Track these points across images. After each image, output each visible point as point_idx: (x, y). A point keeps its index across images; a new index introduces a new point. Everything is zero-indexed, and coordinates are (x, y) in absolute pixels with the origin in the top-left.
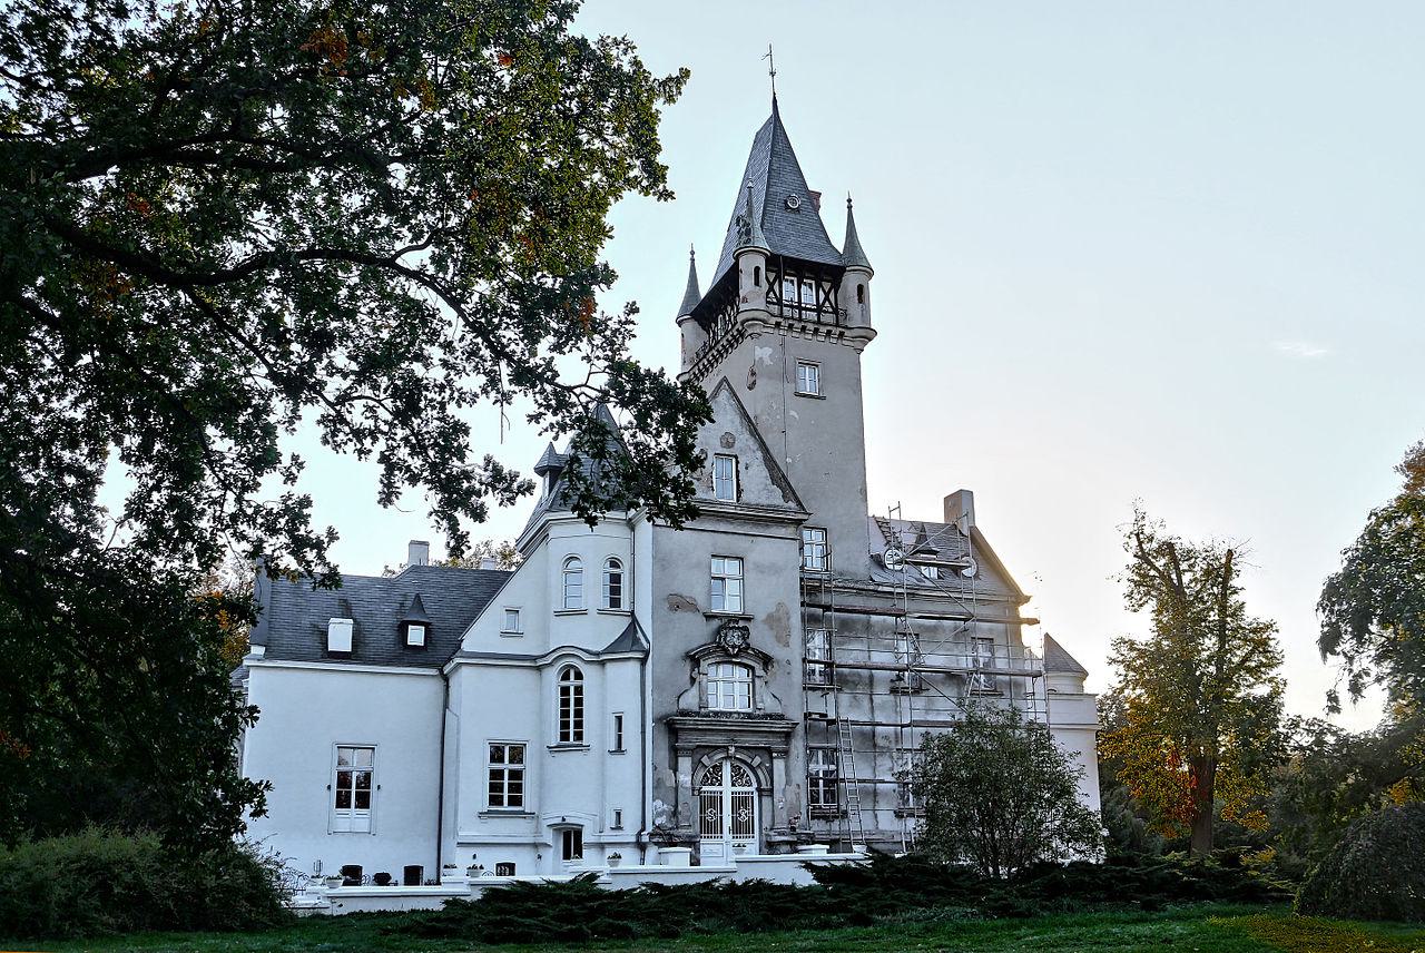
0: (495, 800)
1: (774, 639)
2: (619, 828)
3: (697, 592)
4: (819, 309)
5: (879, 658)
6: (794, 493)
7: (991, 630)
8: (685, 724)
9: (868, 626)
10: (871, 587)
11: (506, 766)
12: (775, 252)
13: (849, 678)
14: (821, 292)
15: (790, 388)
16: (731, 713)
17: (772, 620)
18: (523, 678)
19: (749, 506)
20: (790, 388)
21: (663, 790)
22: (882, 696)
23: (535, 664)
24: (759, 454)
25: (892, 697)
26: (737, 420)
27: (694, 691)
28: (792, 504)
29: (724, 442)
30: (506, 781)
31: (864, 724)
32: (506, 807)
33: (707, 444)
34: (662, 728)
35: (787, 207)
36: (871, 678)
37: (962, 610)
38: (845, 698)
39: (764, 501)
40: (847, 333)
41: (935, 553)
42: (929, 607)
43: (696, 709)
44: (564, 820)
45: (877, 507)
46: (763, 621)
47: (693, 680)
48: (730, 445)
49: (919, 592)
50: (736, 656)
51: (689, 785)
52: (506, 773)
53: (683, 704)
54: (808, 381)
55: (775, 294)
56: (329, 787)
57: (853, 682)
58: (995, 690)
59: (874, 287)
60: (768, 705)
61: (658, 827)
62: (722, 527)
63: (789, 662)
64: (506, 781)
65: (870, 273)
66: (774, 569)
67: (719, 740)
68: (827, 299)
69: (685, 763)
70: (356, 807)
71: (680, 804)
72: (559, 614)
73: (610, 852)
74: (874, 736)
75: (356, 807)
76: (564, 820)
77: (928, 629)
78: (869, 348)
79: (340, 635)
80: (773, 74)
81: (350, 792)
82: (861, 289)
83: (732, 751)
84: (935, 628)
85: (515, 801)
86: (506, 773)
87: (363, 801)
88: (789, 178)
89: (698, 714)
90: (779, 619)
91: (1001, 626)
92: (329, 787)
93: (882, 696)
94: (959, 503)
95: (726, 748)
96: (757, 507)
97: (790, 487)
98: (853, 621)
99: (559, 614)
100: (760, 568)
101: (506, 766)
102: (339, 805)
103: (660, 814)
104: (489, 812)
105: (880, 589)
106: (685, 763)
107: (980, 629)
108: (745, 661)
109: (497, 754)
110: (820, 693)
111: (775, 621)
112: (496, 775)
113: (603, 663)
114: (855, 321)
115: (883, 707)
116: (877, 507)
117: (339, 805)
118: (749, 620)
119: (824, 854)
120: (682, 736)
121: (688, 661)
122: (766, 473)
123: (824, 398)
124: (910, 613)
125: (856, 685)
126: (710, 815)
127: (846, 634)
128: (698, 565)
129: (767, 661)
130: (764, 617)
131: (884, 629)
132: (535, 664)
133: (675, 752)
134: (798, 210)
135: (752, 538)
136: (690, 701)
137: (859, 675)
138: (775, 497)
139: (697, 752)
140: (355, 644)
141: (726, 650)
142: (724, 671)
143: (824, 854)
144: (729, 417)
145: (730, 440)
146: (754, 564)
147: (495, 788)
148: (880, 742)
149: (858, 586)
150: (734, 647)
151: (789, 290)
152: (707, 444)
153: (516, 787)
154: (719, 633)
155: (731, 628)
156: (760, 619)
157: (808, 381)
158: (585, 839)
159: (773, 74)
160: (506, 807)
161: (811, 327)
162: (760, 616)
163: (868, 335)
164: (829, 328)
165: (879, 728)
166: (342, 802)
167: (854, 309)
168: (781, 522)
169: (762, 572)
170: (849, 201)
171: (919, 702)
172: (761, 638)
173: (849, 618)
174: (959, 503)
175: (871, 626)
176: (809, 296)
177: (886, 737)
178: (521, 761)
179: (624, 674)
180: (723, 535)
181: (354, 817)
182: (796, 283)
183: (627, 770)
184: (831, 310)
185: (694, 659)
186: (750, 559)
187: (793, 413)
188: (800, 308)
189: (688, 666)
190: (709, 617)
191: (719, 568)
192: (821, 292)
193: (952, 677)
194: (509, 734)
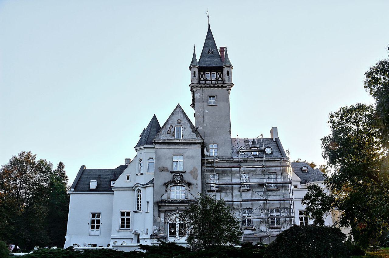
0: (122, 226)
1: (192, 178)
2: (147, 234)
3: (168, 165)
4: (217, 80)
5: (235, 181)
6: (199, 134)
7: (275, 170)
8: (162, 204)
9: (231, 172)
10: (231, 160)
11: (126, 217)
12: (200, 66)
13: (225, 188)
14: (218, 75)
15: (206, 104)
16: (177, 200)
17: (192, 172)
18: (131, 192)
19: (185, 140)
20: (206, 104)
21: (156, 223)
22: (236, 192)
23: (132, 189)
24: (189, 124)
25: (239, 193)
26: (182, 116)
27: (166, 194)
28: (199, 138)
29: (178, 122)
30: (125, 221)
31: (230, 201)
32: (125, 228)
33: (173, 123)
34: (157, 205)
35: (209, 53)
36: (232, 187)
37: (261, 164)
38: (223, 194)
39: (190, 138)
40: (224, 85)
41: (257, 147)
42: (253, 164)
43: (166, 199)
44: (135, 231)
45: (233, 135)
46: (189, 173)
47: (166, 191)
48: (179, 123)
49: (248, 160)
50: (179, 183)
51: (164, 221)
52: (125, 219)
53: (163, 198)
54: (212, 101)
55: (221, 78)
56: (89, 224)
57: (226, 189)
58: (277, 189)
59: (233, 71)
60: (190, 197)
61: (155, 233)
62: (177, 147)
63: (197, 184)
64: (125, 221)
65: (232, 68)
66: (193, 157)
67: (173, 208)
68: (220, 76)
69: (162, 215)
70: (96, 229)
71: (161, 226)
72: (137, 175)
73: (145, 240)
74: (233, 205)
75: (96, 229)
76: (135, 231)
77: (252, 171)
78: (232, 89)
79: (93, 184)
80: (208, 17)
81: (126, 224)
82: (228, 72)
83: (178, 211)
84: (255, 171)
85: (128, 227)
86: (125, 219)
87: (98, 227)
88: (211, 44)
89: (167, 201)
90: (194, 172)
91: (279, 168)
92: (89, 224)
93: (236, 192)
94: (274, 130)
95: (175, 210)
96: (188, 140)
97: (198, 133)
98: (226, 171)
99: (137, 175)
100: (188, 157)
101: (126, 217)
102: (92, 228)
103: (155, 230)
104: (120, 230)
105: (234, 160)
106: (162, 215)
107: (271, 169)
108: (182, 185)
109: (123, 214)
110: (233, 193)
111: (193, 173)
112: (123, 219)
113: (145, 187)
114: (226, 81)
115: (236, 196)
116: (233, 135)
117: (92, 228)
118: (184, 173)
119: (156, 242)
120: (162, 207)
121: (165, 186)
122: (191, 129)
123: (217, 106)
124: (242, 167)
125: (227, 189)
126: (173, 230)
127: (224, 174)
128: (169, 158)
129: (189, 184)
130: (189, 171)
131: (236, 172)
132: (132, 189)
133: (160, 212)
134: (212, 53)
135: (186, 149)
136: (165, 197)
137: (228, 186)
138: (194, 136)
139: (165, 212)
140: (97, 187)
141: (176, 182)
142: (175, 188)
143: (156, 242)
144: (180, 115)
145: (180, 122)
146: (186, 156)
147: (122, 223)
148: (235, 207)
149: (227, 160)
150: (178, 181)
151: (208, 76)
152: (173, 123)
153: (128, 223)
154: (173, 177)
155: (177, 175)
156: (188, 172)
157: (212, 101)
158: (140, 237)
159: (208, 17)
160: (125, 228)
161: (204, 86)
162: (188, 171)
163: (231, 85)
164: (209, 85)
165: (234, 203)
166: (93, 227)
167: (226, 78)
168: (195, 143)
169: (189, 159)
170: (194, 47)
171: (249, 194)
172: (187, 178)
173: (225, 170)
174: (274, 130)
175: (232, 172)
176: (214, 76)
177: (237, 205)
178: (100, 217)
179: (150, 190)
180: (177, 149)
181: (95, 232)
182: (210, 73)
183: (150, 218)
184: (221, 80)
185: (166, 185)
186: (185, 155)
187: (206, 111)
188: (211, 81)
189: (165, 186)
190: (172, 173)
191: (176, 158)
192: (218, 75)
193: (261, 186)
194: (126, 209)
